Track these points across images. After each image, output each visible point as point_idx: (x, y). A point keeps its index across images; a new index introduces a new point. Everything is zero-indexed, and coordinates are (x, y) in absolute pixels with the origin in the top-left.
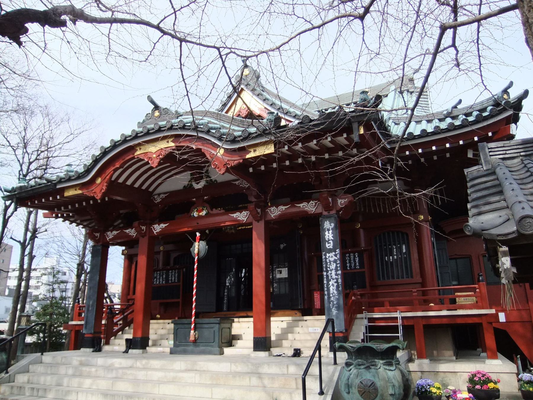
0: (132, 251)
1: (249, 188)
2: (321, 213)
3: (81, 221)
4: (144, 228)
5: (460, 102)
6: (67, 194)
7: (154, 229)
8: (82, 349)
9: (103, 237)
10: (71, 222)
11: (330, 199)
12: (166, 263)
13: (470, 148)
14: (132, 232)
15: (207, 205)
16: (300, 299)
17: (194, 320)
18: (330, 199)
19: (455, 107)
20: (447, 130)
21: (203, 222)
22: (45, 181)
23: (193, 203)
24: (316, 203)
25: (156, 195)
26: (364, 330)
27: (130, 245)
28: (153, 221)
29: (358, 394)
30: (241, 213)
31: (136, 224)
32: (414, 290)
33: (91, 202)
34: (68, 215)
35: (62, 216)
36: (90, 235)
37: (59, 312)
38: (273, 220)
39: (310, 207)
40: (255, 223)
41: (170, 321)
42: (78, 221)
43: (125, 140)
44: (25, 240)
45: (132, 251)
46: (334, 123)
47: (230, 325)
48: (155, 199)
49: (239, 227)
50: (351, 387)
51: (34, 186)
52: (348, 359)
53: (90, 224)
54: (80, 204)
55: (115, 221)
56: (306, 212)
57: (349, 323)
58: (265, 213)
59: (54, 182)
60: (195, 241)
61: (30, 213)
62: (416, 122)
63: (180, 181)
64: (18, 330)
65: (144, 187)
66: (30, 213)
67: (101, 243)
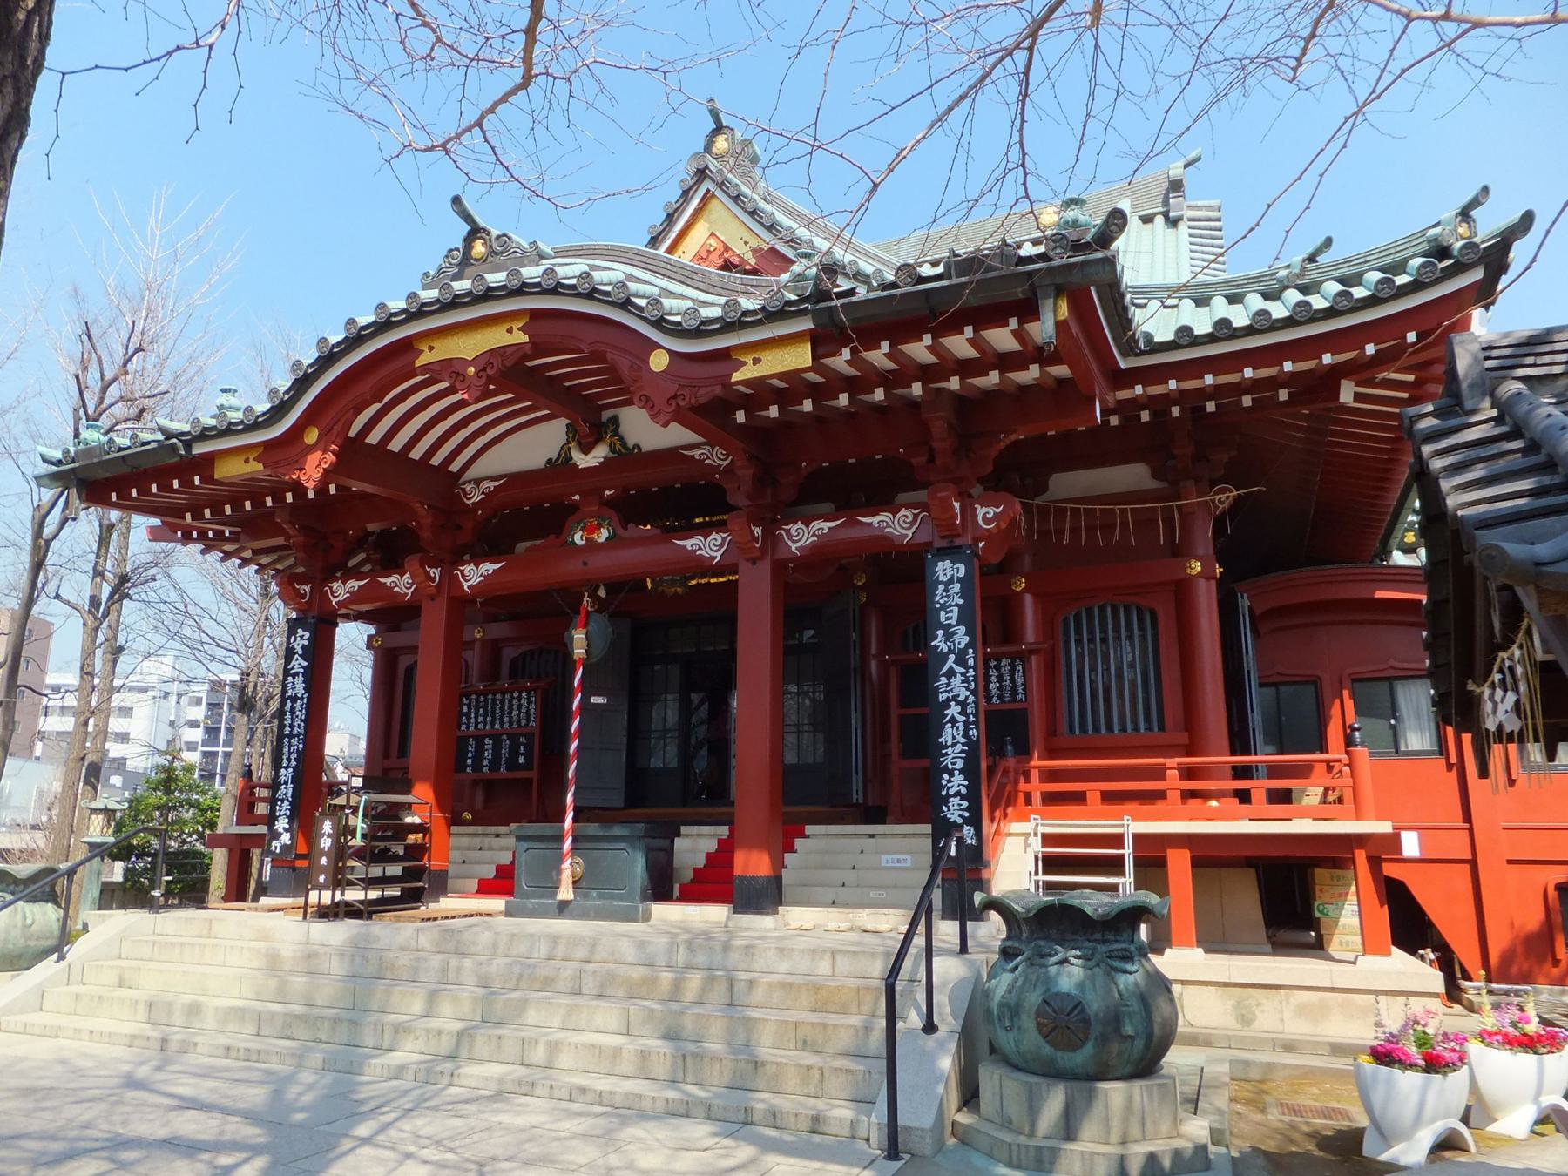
0: (400, 639)
1: (728, 470)
2: (930, 544)
3: (255, 552)
4: (435, 572)
5: (1328, 242)
7: (464, 576)
9: (320, 596)
10: (227, 556)
11: (957, 505)
12: (491, 673)
13: (1345, 377)
14: (400, 584)
15: (611, 513)
17: (573, 828)
18: (957, 505)
19: (1312, 259)
20: (1289, 323)
21: (600, 562)
23: (575, 507)
24: (916, 516)
25: (469, 482)
27: (390, 617)
28: (453, 559)
31: (412, 561)
33: (289, 497)
35: (203, 536)
38: (794, 558)
39: (897, 525)
40: (744, 567)
42: (248, 554)
43: (386, 324)
45: (400, 639)
46: (988, 290)
47: (668, 842)
48: (465, 494)
52: (1008, 938)
54: (258, 502)
55: (351, 554)
56: (888, 539)
58: (771, 538)
62: (1227, 297)
63: (536, 444)
65: (436, 461)
66: (107, 530)
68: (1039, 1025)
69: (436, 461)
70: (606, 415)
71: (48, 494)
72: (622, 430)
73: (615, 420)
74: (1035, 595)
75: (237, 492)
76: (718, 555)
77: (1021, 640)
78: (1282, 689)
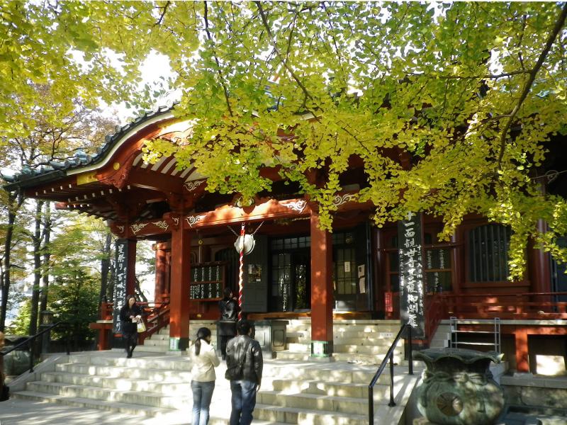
3: (102, 212)
6: (81, 182)
8: (113, 350)
10: (90, 214)
16: (371, 308)
22: (51, 168)
25: (189, 182)
26: (449, 337)
29: (437, 408)
31: (166, 216)
32: (518, 295)
33: (111, 191)
34: (85, 206)
35: (78, 208)
36: (114, 228)
37: (108, 294)
41: (212, 321)
44: (38, 233)
49: (294, 218)
50: (429, 400)
51: (40, 174)
53: (112, 215)
57: (431, 329)
59: (62, 169)
60: (240, 235)
61: (41, 204)
64: (41, 328)
67: (125, 238)
68: (439, 406)
69: (174, 173)
71: (371, 183)
75: (89, 189)
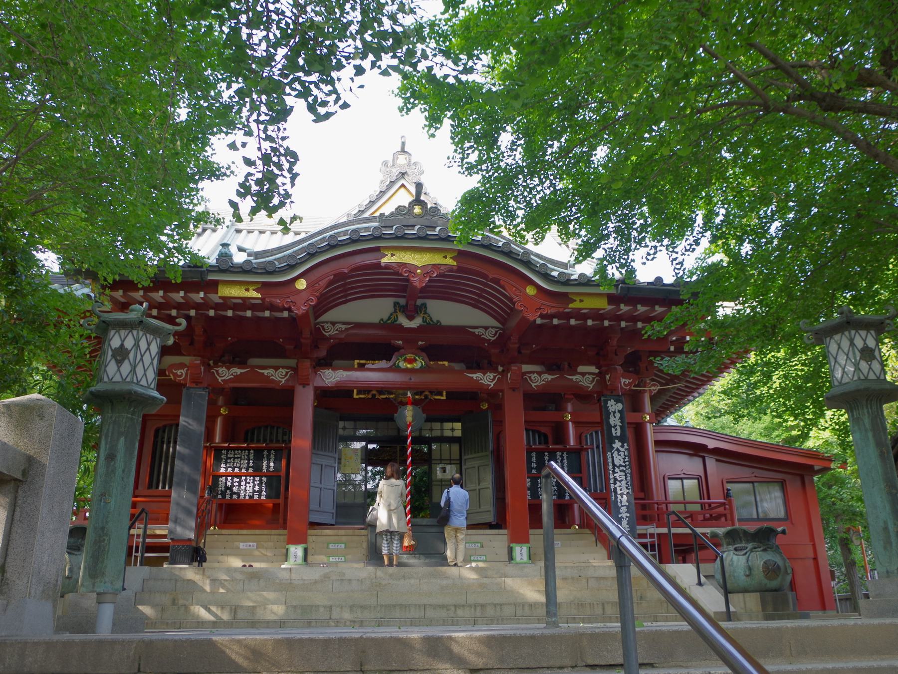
7: (218, 374)
15: (424, 354)
23: (397, 349)
25: (327, 322)
30: (228, 369)
70: (419, 302)
72: (428, 311)
73: (424, 306)
74: (573, 422)
76: (492, 384)
77: (568, 443)
78: (685, 481)
